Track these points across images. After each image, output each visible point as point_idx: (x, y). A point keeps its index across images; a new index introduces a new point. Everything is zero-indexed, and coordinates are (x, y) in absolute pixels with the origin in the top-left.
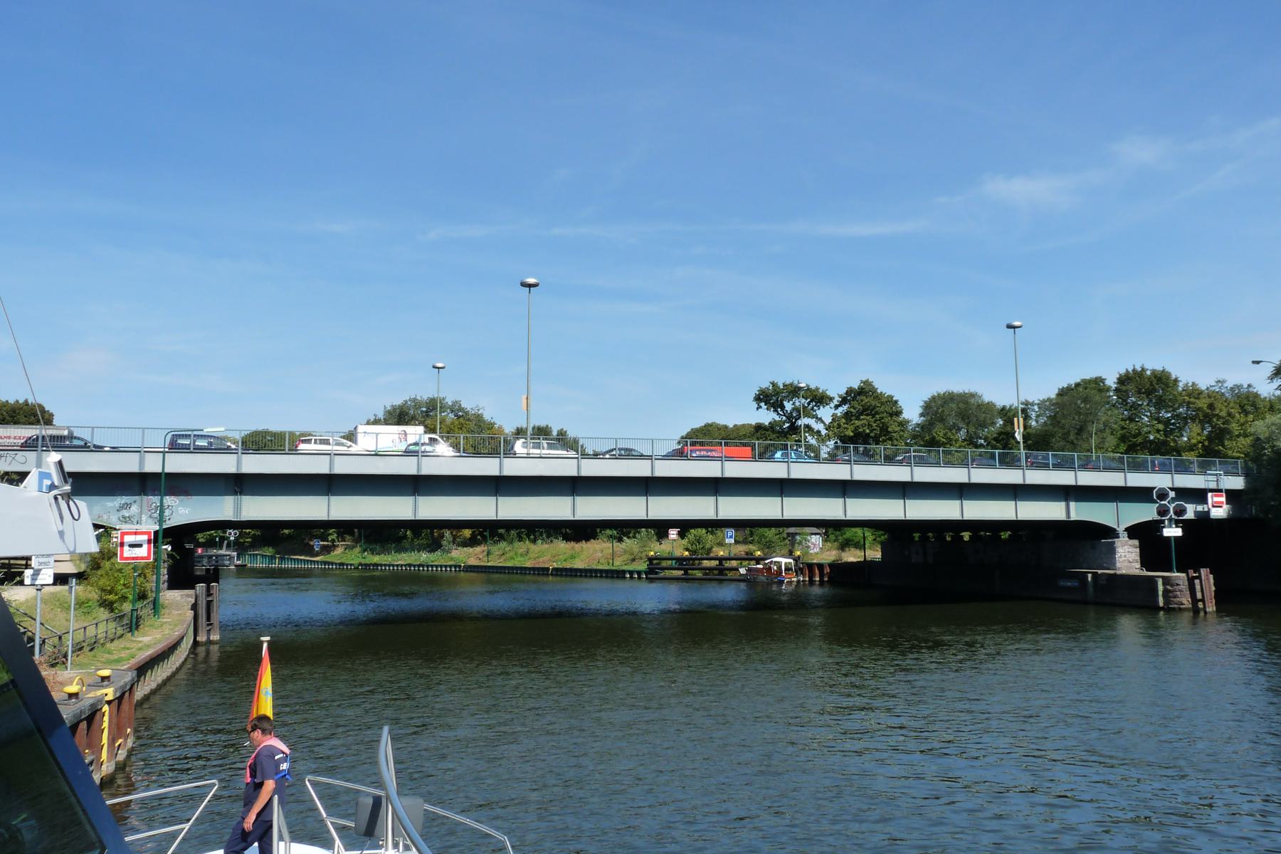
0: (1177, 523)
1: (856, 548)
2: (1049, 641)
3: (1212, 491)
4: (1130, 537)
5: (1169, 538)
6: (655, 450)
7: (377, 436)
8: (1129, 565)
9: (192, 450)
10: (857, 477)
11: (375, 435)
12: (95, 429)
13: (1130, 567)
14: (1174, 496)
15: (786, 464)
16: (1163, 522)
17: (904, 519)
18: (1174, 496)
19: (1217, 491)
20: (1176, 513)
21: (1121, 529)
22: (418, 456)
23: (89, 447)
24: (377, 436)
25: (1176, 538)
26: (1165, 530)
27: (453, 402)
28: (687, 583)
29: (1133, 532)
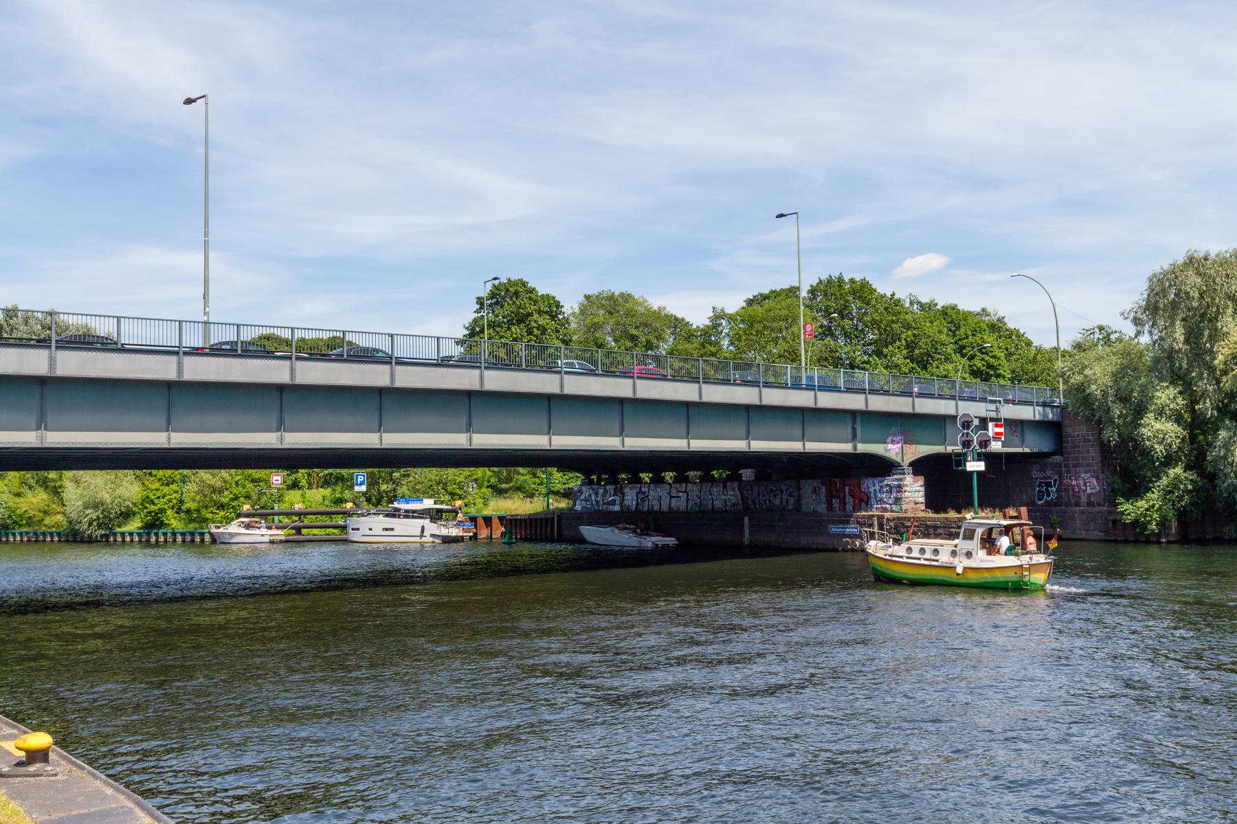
0: (979, 457)
1: (1101, 453)
2: (939, 578)
3: (992, 420)
4: (916, 473)
5: (971, 473)
6: (228, 335)
7: (119, 322)
8: (915, 506)
9: (239, 352)
10: (300, 379)
11: (178, 323)
12: (184, 323)
13: (916, 509)
14: (978, 424)
15: (287, 363)
16: (965, 454)
17: (687, 449)
18: (978, 424)
19: (996, 421)
20: (981, 446)
21: (905, 464)
22: (480, 367)
23: (730, 380)
24: (119, 322)
25: (979, 473)
26: (968, 464)
27: (477, 303)
28: (344, 544)
29: (919, 466)
